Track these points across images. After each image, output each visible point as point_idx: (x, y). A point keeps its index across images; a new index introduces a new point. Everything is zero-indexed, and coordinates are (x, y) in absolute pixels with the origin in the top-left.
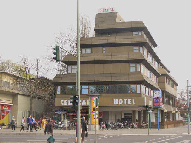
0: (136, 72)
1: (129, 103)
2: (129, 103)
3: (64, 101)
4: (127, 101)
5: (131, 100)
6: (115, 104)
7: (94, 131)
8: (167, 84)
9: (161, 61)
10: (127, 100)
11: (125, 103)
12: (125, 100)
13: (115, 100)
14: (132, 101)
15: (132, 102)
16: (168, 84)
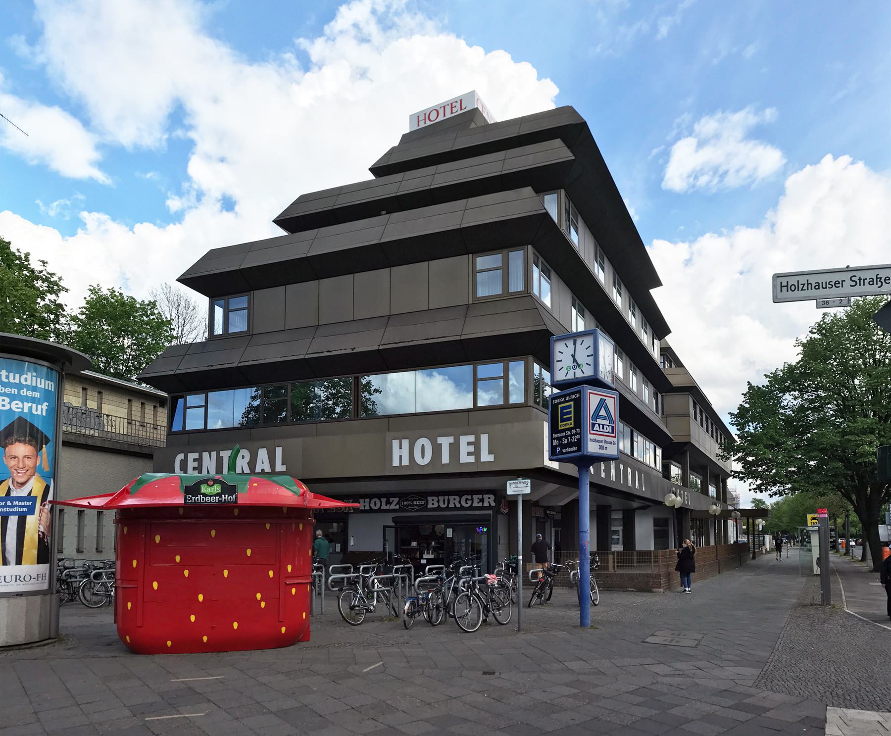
0: (507, 297)
1: (465, 458)
2: (465, 458)
3: (186, 457)
4: (455, 449)
5: (472, 438)
6: (396, 463)
7: (479, 377)
8: (715, 440)
9: (819, 553)
10: (451, 439)
11: (445, 459)
12: (445, 442)
13: (396, 443)
14: (477, 444)
15: (477, 453)
16: (702, 425)
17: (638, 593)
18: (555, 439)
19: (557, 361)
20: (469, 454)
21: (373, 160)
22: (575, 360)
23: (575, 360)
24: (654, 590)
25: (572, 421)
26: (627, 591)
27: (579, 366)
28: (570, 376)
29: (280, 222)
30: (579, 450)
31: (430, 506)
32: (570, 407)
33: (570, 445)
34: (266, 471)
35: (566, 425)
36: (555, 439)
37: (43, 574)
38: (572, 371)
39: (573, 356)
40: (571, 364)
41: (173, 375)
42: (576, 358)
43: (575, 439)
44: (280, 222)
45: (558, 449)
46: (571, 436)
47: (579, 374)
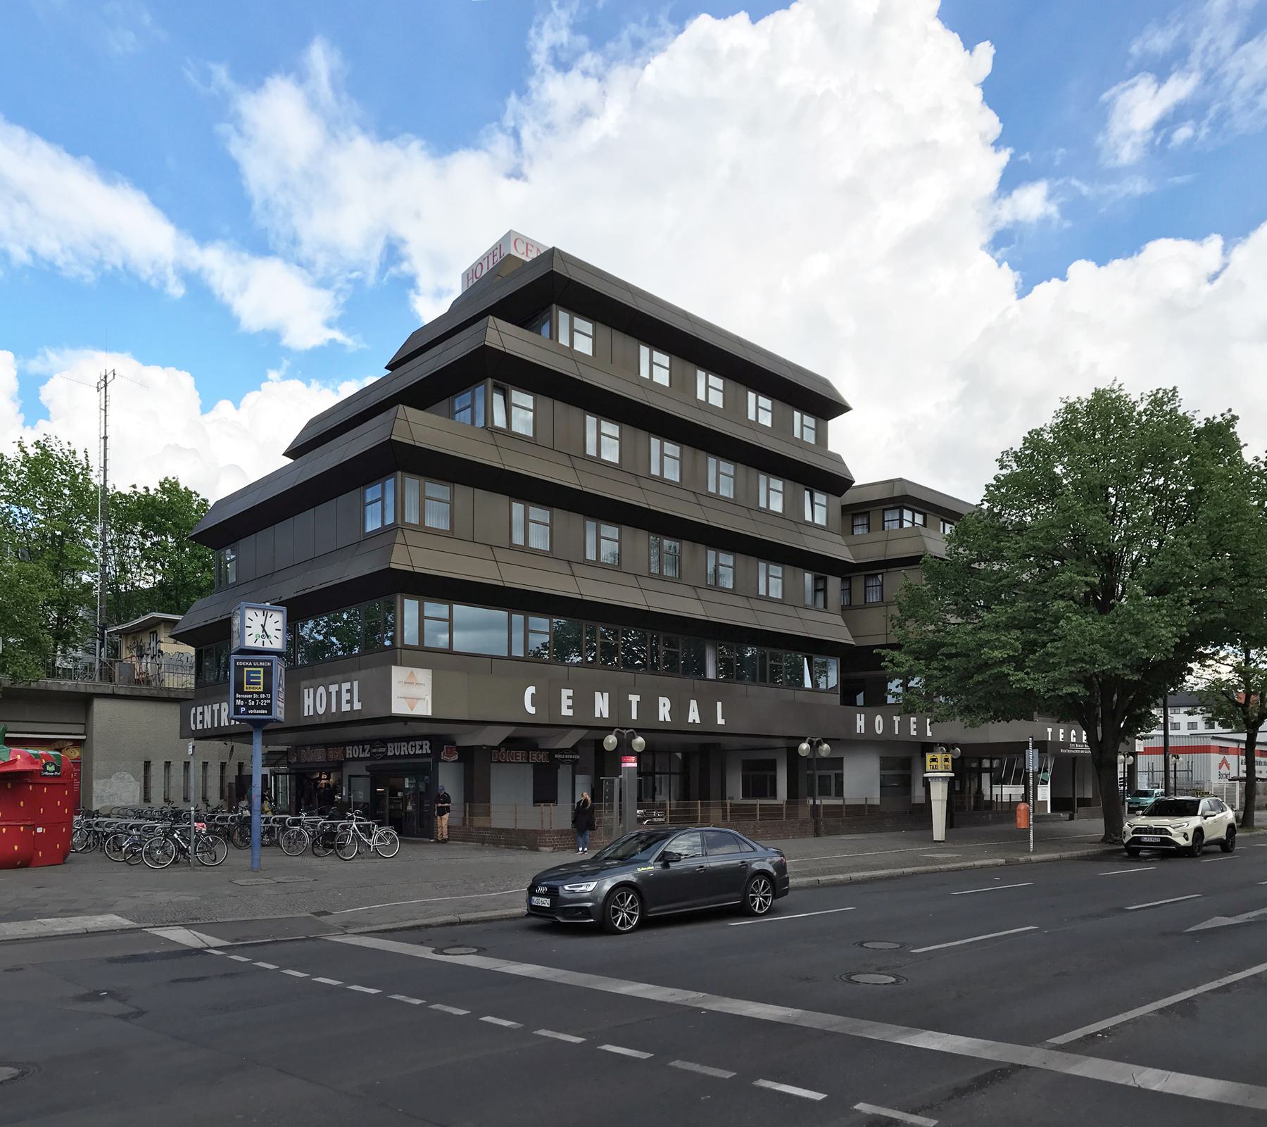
17: (529, 852)
18: (238, 699)
19: (247, 627)
20: (569, 707)
21: (286, 443)
22: (264, 630)
23: (264, 630)
24: (541, 848)
25: (262, 686)
26: (521, 849)
27: (268, 637)
28: (259, 645)
29: (287, 454)
30: (270, 713)
31: (389, 754)
32: (259, 672)
33: (259, 708)
34: (349, 688)
35: (253, 688)
36: (238, 699)
37: (250, 836)
38: (260, 640)
39: (263, 626)
40: (261, 634)
41: (848, 628)
42: (265, 628)
43: (264, 703)
44: (287, 454)
45: (243, 710)
46: (260, 699)
47: (268, 645)
